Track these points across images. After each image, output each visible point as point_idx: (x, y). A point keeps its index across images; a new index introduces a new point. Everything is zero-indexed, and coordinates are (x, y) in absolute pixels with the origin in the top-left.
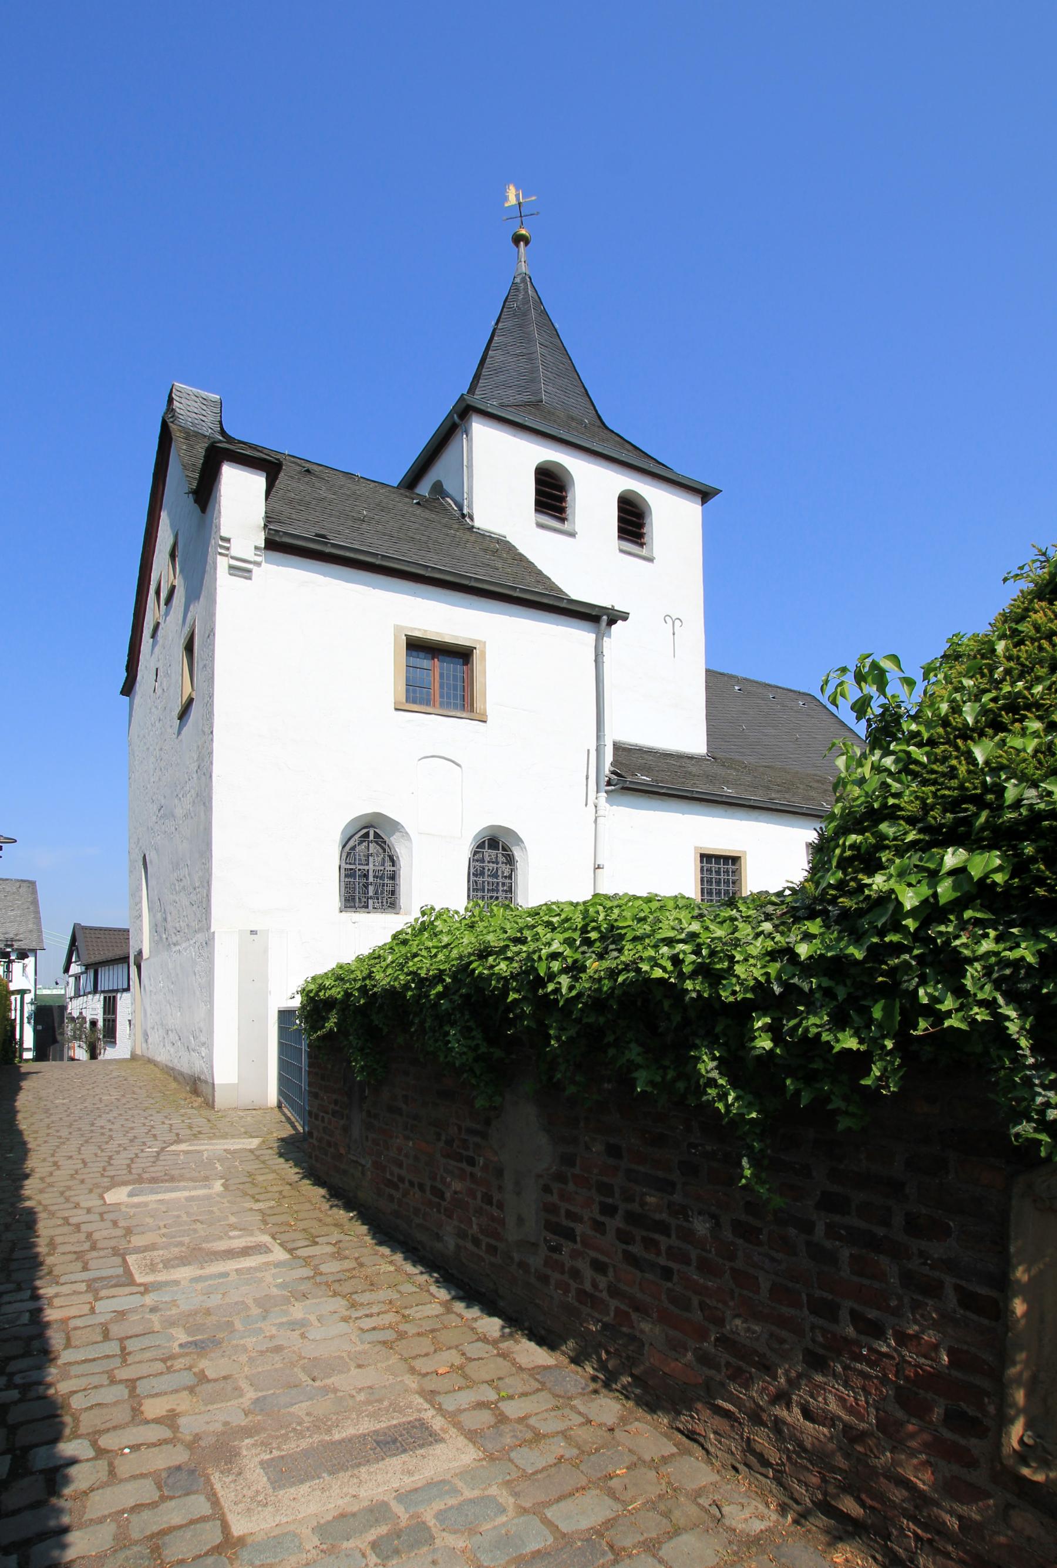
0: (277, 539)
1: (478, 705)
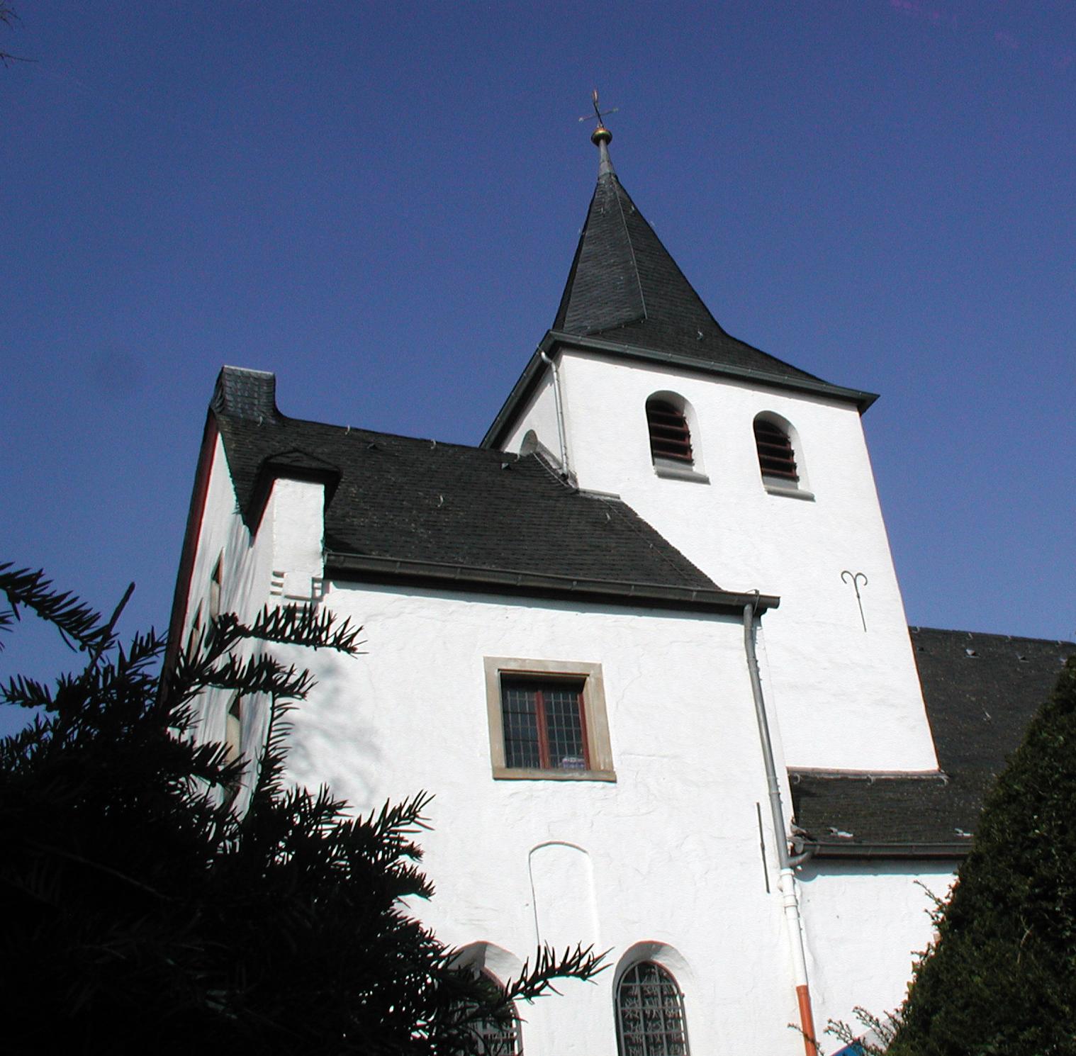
0: (337, 565)
1: (597, 757)
